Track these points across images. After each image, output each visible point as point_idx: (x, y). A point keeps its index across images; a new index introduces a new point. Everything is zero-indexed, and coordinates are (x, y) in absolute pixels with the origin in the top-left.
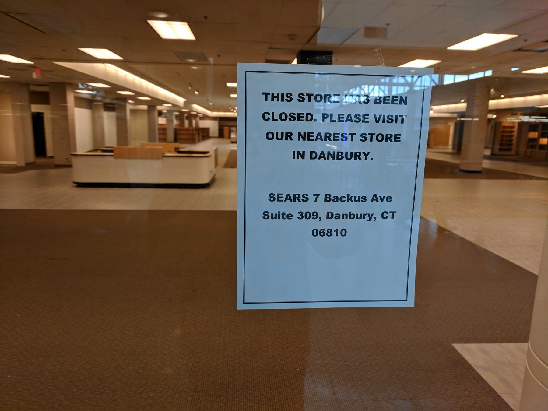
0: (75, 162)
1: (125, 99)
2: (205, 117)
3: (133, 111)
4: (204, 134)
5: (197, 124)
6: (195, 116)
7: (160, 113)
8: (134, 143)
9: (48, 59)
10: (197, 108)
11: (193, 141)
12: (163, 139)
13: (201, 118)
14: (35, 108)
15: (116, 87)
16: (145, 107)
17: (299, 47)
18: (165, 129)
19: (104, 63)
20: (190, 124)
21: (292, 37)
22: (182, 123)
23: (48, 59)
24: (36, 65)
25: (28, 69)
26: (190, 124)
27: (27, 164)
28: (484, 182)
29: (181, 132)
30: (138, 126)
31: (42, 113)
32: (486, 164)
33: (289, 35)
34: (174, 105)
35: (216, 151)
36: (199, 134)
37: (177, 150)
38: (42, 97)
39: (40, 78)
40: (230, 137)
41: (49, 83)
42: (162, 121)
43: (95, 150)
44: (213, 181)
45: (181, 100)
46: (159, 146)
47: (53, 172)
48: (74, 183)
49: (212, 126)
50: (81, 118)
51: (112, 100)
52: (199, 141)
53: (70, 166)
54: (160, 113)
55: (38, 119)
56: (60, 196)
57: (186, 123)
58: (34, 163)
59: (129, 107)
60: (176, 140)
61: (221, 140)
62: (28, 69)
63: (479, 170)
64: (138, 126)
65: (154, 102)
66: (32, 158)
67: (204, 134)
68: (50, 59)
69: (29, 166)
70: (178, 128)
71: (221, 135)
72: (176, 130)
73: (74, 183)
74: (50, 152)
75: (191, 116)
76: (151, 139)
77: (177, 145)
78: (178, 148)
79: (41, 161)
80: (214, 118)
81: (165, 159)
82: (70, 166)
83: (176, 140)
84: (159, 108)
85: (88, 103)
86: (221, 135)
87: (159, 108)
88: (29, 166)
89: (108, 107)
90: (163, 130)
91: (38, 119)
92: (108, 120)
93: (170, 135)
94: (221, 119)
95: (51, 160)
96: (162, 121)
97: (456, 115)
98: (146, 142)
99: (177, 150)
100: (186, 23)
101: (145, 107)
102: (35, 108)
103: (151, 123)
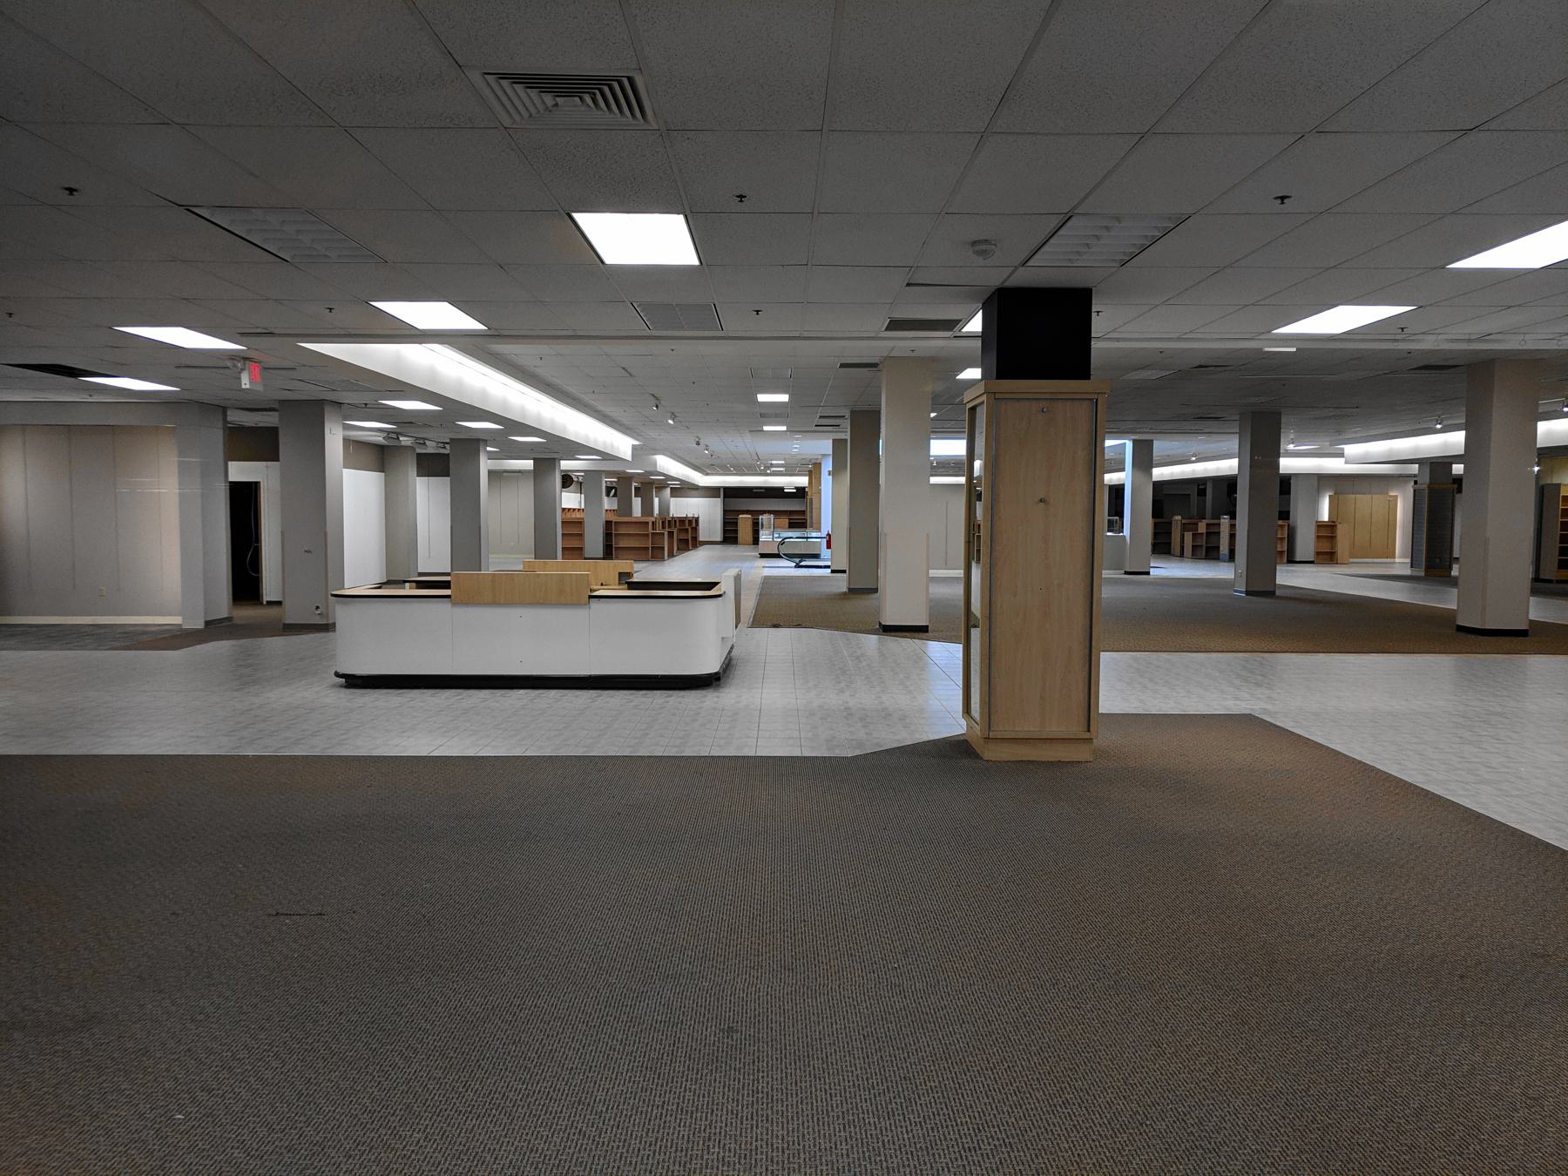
0: (343, 615)
1: (473, 444)
2: (684, 489)
3: (492, 474)
4: (685, 535)
5: (665, 508)
6: (661, 486)
7: (567, 480)
8: (496, 562)
9: (279, 335)
10: (667, 465)
11: (655, 554)
12: (575, 551)
13: (676, 492)
14: (240, 471)
15: (454, 409)
16: (528, 464)
17: (995, 276)
18: (580, 523)
19: (430, 350)
20: (647, 508)
21: (981, 246)
22: (626, 507)
23: (279, 335)
24: (251, 354)
25: (229, 364)
26: (647, 508)
27: (207, 623)
28: (1539, 664)
29: (623, 531)
30: (508, 515)
31: (257, 484)
32: (1539, 610)
33: (974, 243)
34: (606, 457)
35: (738, 578)
36: (671, 534)
37: (625, 578)
38: (260, 444)
39: (260, 388)
40: (756, 541)
41: (282, 402)
42: (570, 500)
43: (389, 583)
44: (728, 665)
45: (622, 445)
46: (559, 567)
47: (276, 645)
48: (337, 675)
49: (707, 512)
50: (357, 493)
51: (442, 446)
52: (671, 555)
53: (328, 628)
54: (567, 480)
55: (244, 500)
56: (303, 715)
57: (637, 503)
58: (229, 619)
59: (485, 464)
60: (609, 553)
61: (731, 550)
62: (229, 364)
63: (1524, 627)
64: (508, 515)
65: (550, 452)
66: (222, 605)
67: (685, 535)
68: (296, 335)
69: (215, 629)
70: (614, 519)
71: (730, 536)
72: (608, 524)
73: (337, 675)
74: (270, 589)
75: (650, 485)
76: (542, 550)
77: (622, 565)
78: (629, 575)
79: (247, 613)
80: (712, 492)
81: (595, 604)
82: (328, 628)
83: (609, 553)
84: (566, 465)
85: (380, 456)
86: (730, 536)
87: (566, 465)
88: (215, 629)
89: (432, 465)
90: (574, 525)
91: (244, 500)
92: (429, 499)
93: (594, 539)
94: (730, 493)
95: (273, 612)
96: (570, 500)
97: (1415, 468)
98: (530, 558)
99: (625, 578)
100: (608, 261)
101: (528, 464)
102: (240, 471)
103: (544, 506)
